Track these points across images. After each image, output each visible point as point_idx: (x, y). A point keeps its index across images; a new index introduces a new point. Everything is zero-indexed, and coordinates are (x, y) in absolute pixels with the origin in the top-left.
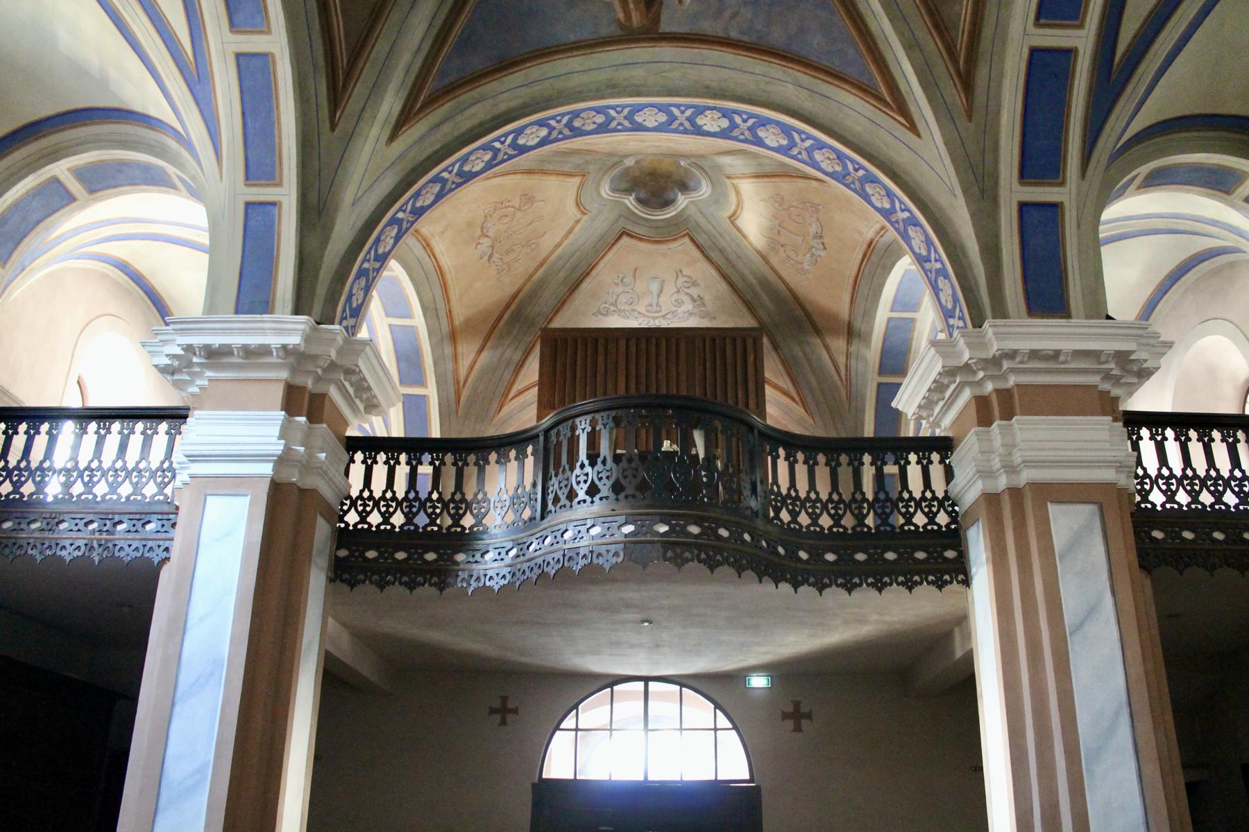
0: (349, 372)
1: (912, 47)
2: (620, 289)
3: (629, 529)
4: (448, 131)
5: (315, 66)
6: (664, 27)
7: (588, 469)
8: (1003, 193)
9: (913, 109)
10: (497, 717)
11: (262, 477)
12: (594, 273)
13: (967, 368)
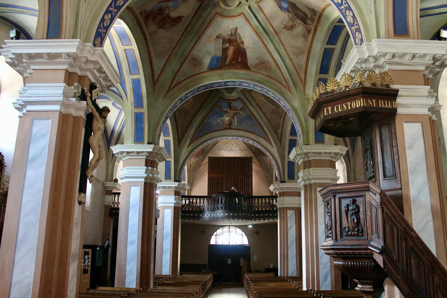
0: (183, 188)
1: (272, 136)
2: (224, 146)
3: (227, 214)
4: (196, 144)
5: (176, 139)
6: (232, 128)
7: (221, 205)
8: (286, 160)
9: (272, 143)
10: (202, 233)
11: (173, 206)
12: (219, 143)
13: (300, 154)
